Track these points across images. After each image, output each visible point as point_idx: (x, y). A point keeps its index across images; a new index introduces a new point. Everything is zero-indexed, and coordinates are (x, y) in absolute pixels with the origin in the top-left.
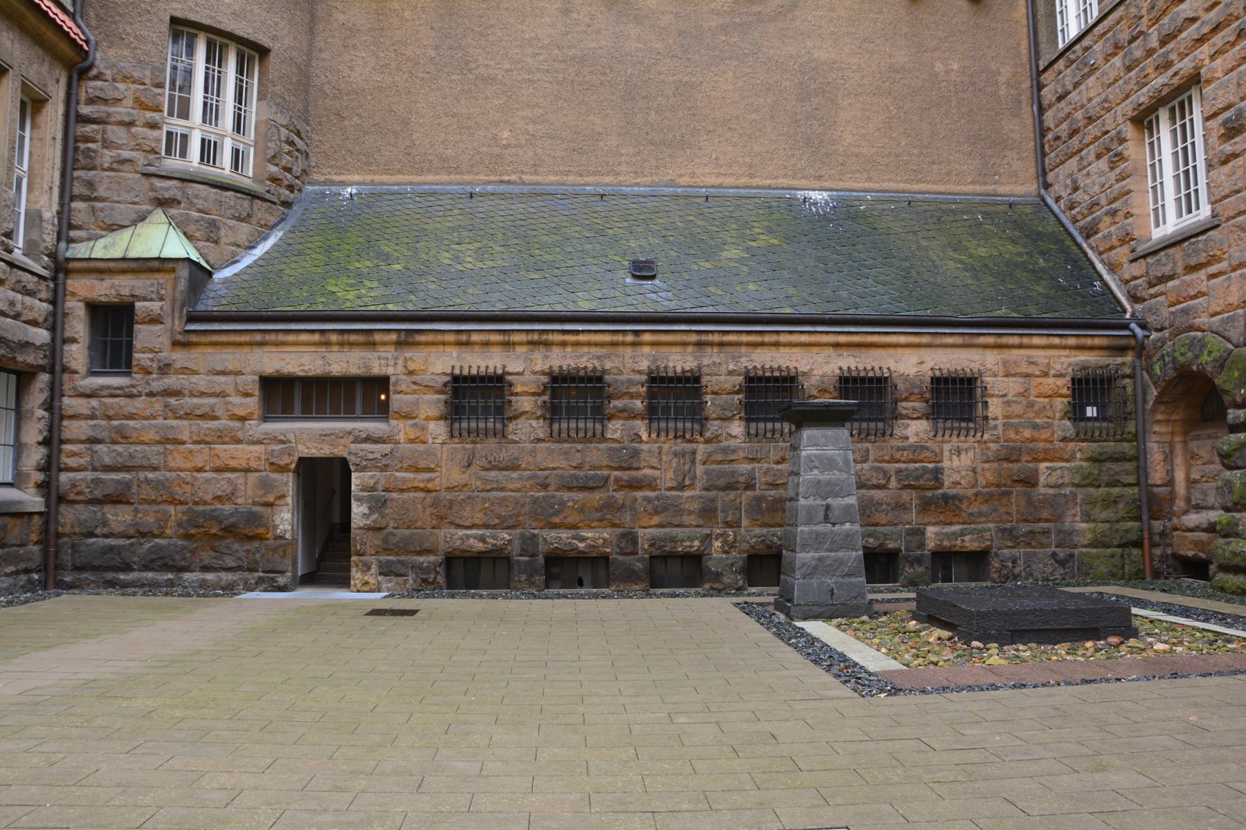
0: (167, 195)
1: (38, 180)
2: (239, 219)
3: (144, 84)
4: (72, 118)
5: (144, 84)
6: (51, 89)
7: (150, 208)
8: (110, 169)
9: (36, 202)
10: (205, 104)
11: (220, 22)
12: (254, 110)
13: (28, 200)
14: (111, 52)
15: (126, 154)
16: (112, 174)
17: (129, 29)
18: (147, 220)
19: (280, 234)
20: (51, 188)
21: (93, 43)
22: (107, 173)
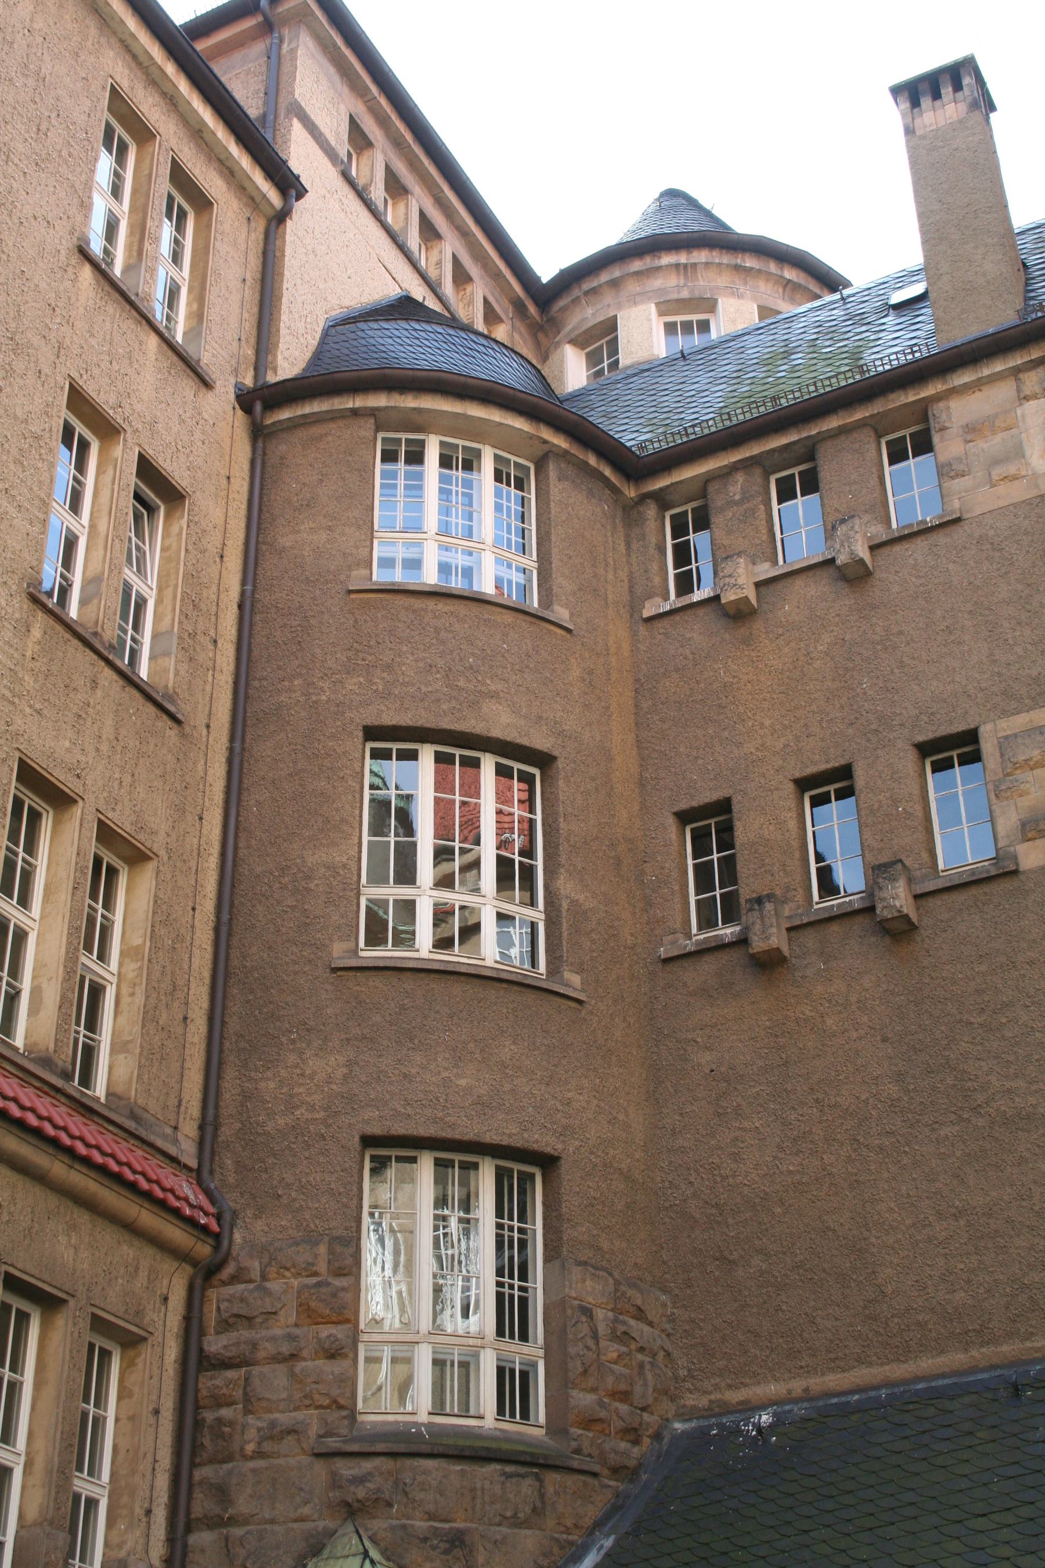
0: (361, 1493)
1: (125, 1500)
2: (516, 1523)
3: (315, 1274)
4: (195, 1361)
5: (315, 1274)
6: (152, 1316)
7: (330, 1524)
8: (259, 1454)
9: (120, 1546)
10: (500, 1296)
11: (452, 1126)
12: (540, 1285)
13: (106, 1544)
14: (259, 1225)
15: (284, 1418)
16: (260, 1463)
17: (289, 1178)
18: (326, 1553)
19: (608, 1543)
20: (149, 1512)
21: (227, 1216)
22: (251, 1464)
